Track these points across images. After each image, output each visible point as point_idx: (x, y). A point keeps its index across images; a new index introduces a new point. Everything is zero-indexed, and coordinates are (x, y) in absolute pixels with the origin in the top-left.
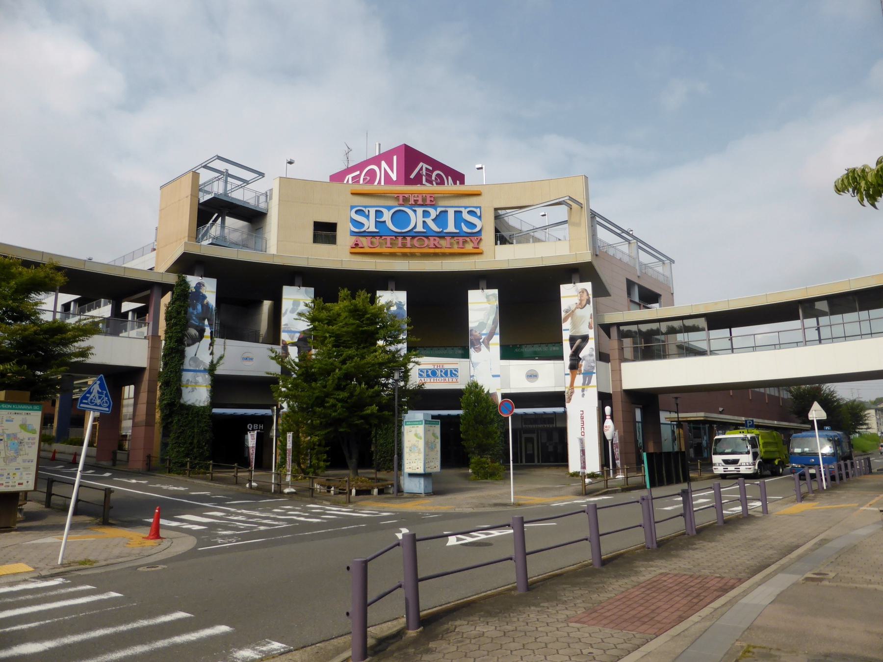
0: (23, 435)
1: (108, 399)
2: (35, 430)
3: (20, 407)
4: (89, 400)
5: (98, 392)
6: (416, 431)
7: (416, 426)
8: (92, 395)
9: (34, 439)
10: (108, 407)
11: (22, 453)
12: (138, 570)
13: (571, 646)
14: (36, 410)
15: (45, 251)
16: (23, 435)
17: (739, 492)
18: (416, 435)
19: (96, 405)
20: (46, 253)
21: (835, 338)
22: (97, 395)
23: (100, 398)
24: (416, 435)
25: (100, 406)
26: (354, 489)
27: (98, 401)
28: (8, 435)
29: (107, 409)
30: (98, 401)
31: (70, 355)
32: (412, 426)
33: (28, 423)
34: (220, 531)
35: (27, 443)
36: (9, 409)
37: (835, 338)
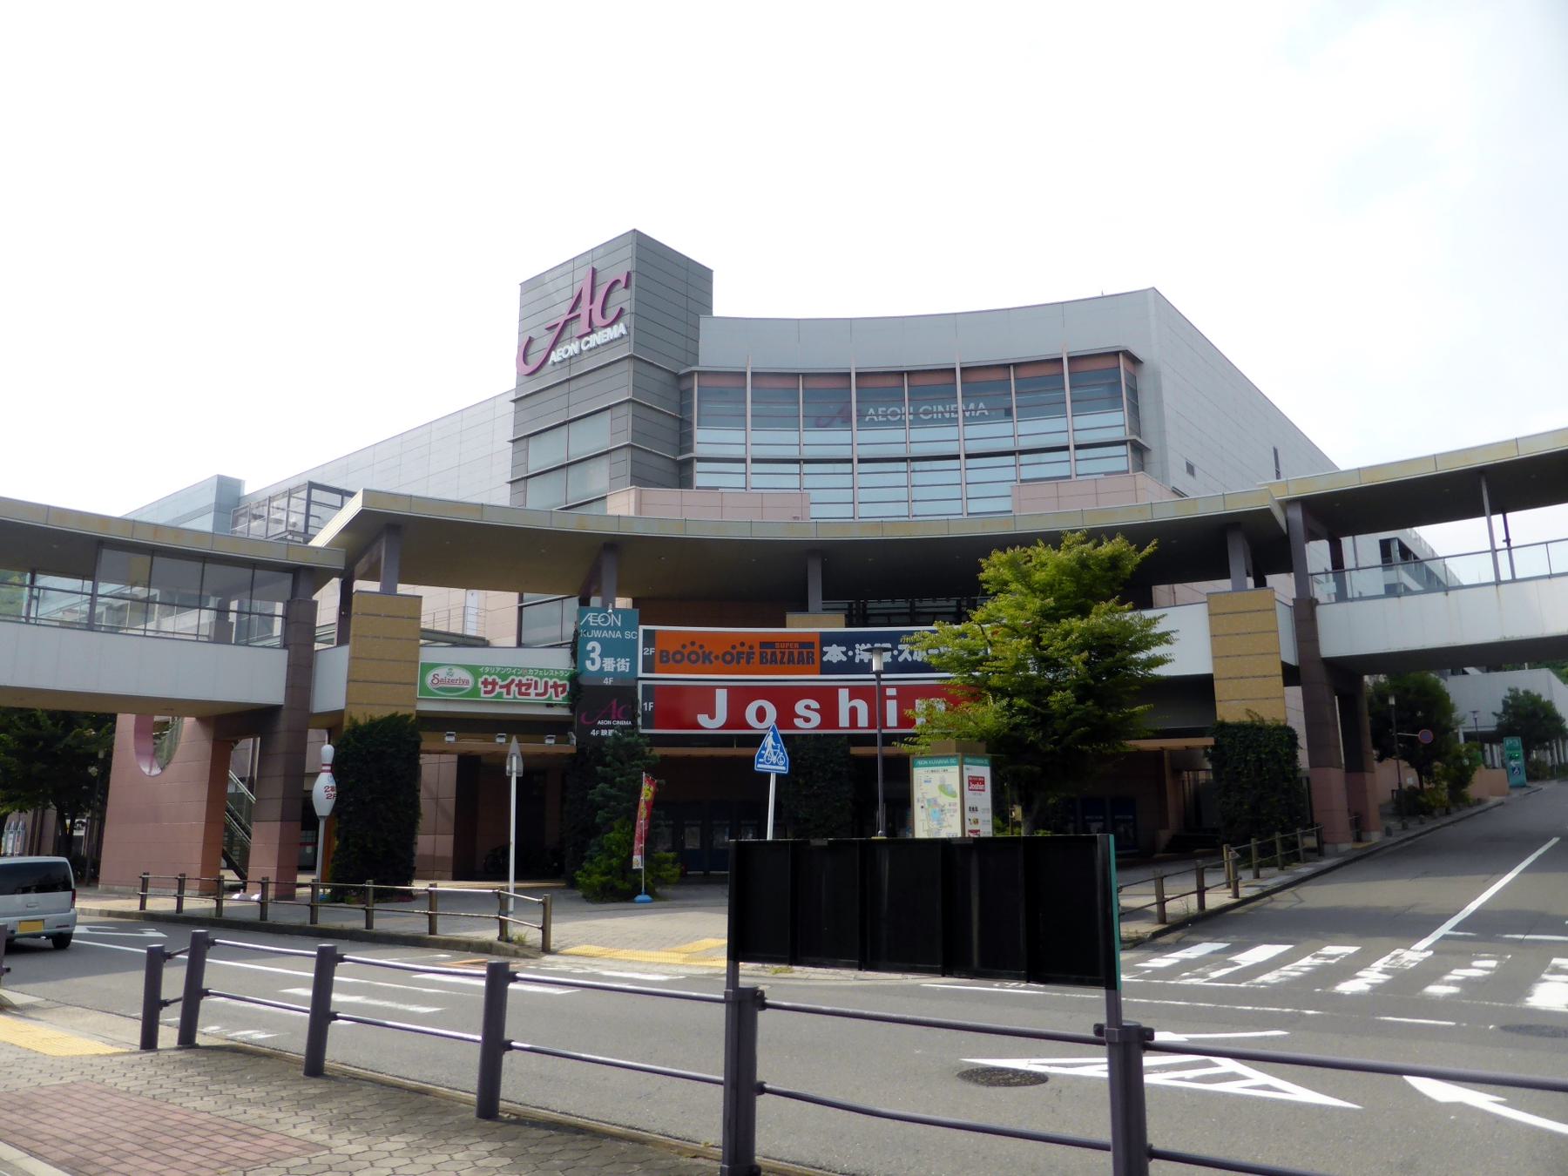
0: (945, 800)
1: (784, 755)
2: (955, 792)
3: (937, 762)
4: (765, 757)
5: (773, 747)
6: (942, 780)
7: (940, 768)
8: (767, 751)
9: (955, 804)
10: (785, 765)
11: (945, 824)
12: (1405, 1081)
13: (416, 1162)
14: (953, 764)
15: (1360, 466)
16: (945, 800)
17: (177, 887)
18: (943, 788)
19: (772, 764)
20: (1438, 455)
21: (957, 484)
22: (772, 751)
23: (775, 753)
24: (943, 788)
25: (777, 764)
26: (222, 872)
27: (774, 759)
28: (929, 801)
29: (784, 768)
30: (774, 759)
31: (1135, 663)
32: (931, 768)
33: (947, 783)
34: (1186, 978)
35: (949, 811)
36: (925, 766)
37: (957, 484)
